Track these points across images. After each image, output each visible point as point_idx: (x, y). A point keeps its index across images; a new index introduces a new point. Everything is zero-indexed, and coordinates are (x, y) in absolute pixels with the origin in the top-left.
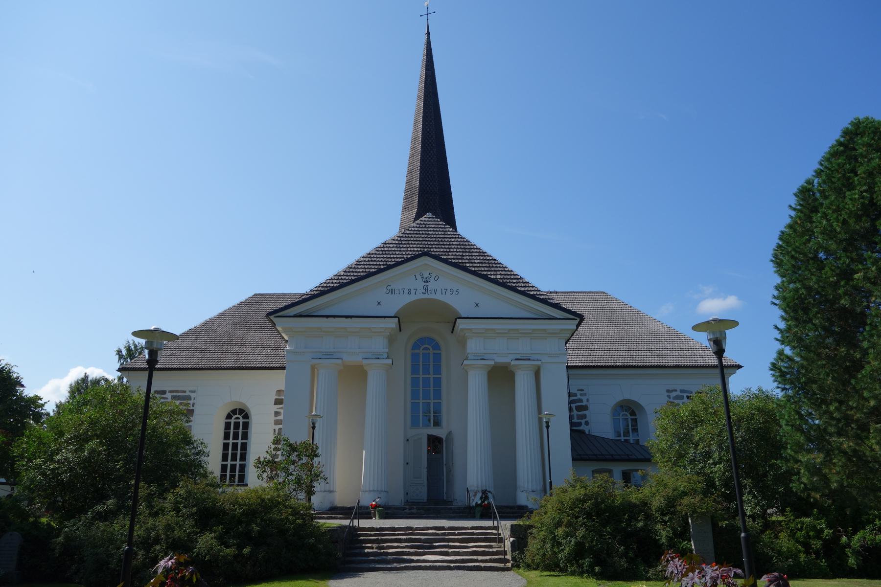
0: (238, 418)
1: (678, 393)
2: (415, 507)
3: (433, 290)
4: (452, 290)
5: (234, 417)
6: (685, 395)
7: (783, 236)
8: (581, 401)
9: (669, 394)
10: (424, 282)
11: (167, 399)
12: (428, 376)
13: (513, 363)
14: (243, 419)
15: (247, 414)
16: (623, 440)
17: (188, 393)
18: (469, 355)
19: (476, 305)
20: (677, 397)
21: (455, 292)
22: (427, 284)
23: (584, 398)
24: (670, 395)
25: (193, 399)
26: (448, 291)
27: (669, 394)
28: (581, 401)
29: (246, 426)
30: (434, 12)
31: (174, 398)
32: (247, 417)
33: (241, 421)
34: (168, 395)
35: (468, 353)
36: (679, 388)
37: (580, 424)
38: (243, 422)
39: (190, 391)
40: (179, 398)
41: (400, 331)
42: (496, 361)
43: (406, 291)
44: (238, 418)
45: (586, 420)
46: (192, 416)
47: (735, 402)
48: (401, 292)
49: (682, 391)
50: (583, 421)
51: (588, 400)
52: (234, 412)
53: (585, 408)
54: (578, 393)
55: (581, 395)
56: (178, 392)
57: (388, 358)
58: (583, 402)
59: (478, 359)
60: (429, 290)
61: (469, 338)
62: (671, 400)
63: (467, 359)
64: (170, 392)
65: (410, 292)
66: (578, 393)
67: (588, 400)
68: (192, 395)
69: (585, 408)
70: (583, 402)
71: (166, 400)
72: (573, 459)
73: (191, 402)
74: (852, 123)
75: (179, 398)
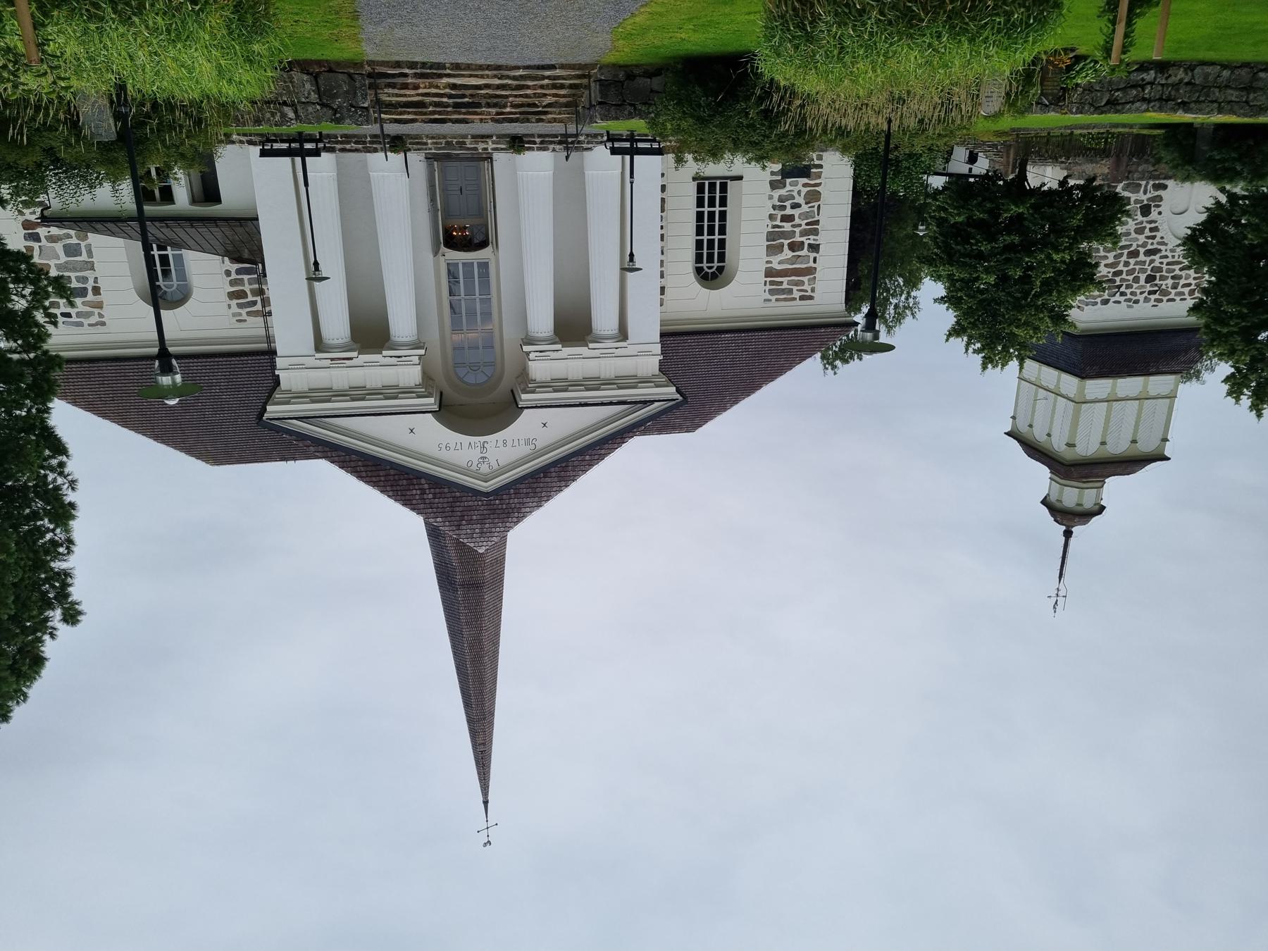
0: (710, 268)
1: (86, 322)
2: (480, 151)
3: (473, 447)
4: (448, 449)
5: (714, 269)
6: (74, 319)
7: (63, 513)
8: (240, 306)
9: (101, 319)
10: (486, 458)
11: (807, 291)
12: (712, 237)
13: (354, 354)
14: (702, 267)
15: (699, 274)
16: (169, 248)
17: (773, 298)
18: (417, 362)
19: (414, 431)
20: (88, 315)
21: (444, 447)
22: (482, 455)
23: (235, 309)
24: (100, 318)
25: (767, 291)
26: (452, 449)
27: (101, 319)
28: (240, 306)
29: (699, 258)
30: (497, 824)
31: (790, 291)
32: (699, 271)
33: (705, 265)
34: (796, 294)
35: (419, 364)
36: (86, 329)
37: (238, 272)
38: (702, 263)
39: (770, 300)
40: (783, 291)
41: (512, 391)
42: (381, 355)
43: (509, 443)
44: (710, 268)
45: (230, 278)
46: (29, 687)
47: (837, 150)
48: (516, 443)
49: (80, 325)
50: (234, 276)
51: (229, 306)
52: (714, 276)
53: (232, 295)
54: (244, 316)
55: (240, 314)
56: (785, 300)
57: (528, 353)
58: (237, 304)
59: (405, 356)
60: (479, 447)
61: (420, 385)
62: (96, 311)
63: (420, 356)
64: (794, 299)
65: (505, 443)
66: (244, 316)
67: (229, 306)
68: (768, 296)
69: (232, 295)
70: (237, 304)
71: (799, 288)
72: (257, 219)
73: (768, 287)
74: (78, 621)
75: (783, 291)
